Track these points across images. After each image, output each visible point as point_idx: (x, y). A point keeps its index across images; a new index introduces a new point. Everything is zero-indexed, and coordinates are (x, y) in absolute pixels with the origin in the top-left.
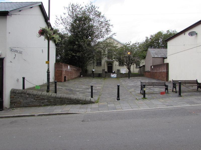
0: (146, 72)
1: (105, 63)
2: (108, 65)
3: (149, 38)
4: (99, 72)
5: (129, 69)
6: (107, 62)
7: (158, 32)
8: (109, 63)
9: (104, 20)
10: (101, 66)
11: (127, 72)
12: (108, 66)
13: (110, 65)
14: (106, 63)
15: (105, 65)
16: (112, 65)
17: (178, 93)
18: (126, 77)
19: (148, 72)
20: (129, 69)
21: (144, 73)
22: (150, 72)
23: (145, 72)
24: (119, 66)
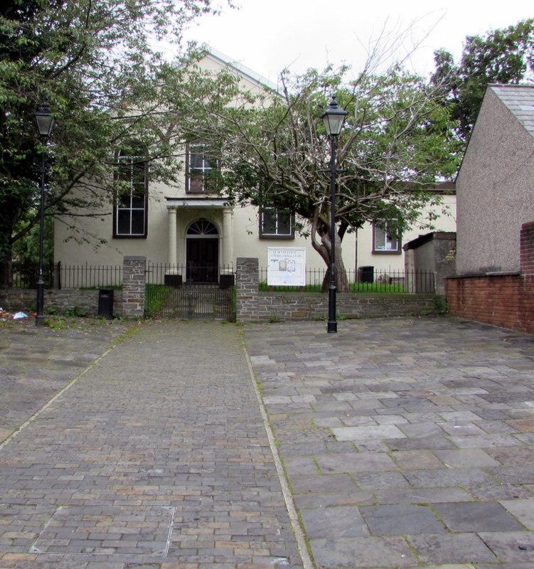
0: (472, 277)
1: (167, 220)
2: (190, 232)
3: (457, 62)
4: (107, 280)
5: (330, 255)
6: (182, 213)
7: (515, 24)
8: (199, 223)
9: (282, 138)
10: (145, 237)
11: (319, 279)
12: (190, 242)
13: (202, 236)
14: (174, 217)
15: (167, 230)
16: (216, 231)
17: (347, 270)
18: (305, 316)
19: (494, 278)
20: (330, 255)
21: (453, 284)
22: (516, 276)
23: (461, 280)
24: (262, 238)
